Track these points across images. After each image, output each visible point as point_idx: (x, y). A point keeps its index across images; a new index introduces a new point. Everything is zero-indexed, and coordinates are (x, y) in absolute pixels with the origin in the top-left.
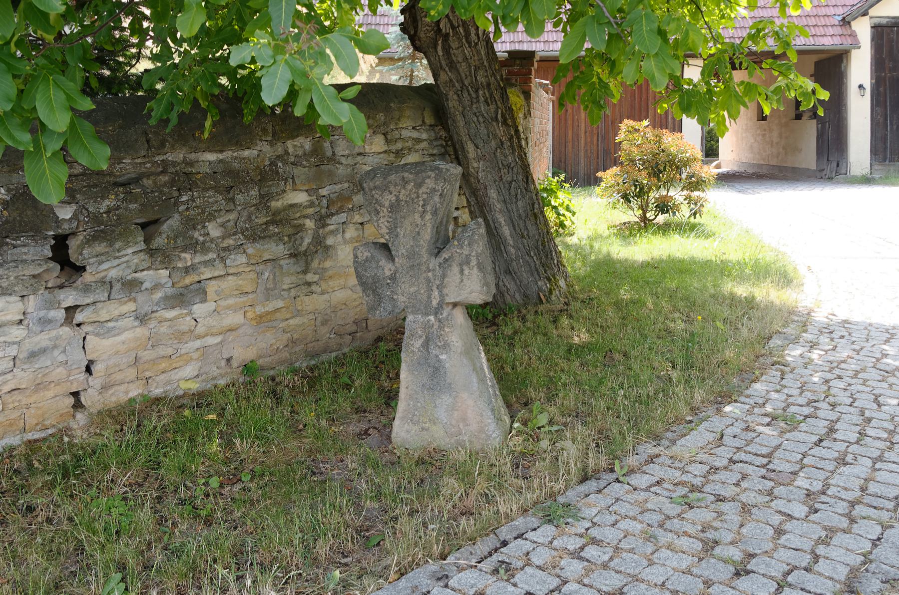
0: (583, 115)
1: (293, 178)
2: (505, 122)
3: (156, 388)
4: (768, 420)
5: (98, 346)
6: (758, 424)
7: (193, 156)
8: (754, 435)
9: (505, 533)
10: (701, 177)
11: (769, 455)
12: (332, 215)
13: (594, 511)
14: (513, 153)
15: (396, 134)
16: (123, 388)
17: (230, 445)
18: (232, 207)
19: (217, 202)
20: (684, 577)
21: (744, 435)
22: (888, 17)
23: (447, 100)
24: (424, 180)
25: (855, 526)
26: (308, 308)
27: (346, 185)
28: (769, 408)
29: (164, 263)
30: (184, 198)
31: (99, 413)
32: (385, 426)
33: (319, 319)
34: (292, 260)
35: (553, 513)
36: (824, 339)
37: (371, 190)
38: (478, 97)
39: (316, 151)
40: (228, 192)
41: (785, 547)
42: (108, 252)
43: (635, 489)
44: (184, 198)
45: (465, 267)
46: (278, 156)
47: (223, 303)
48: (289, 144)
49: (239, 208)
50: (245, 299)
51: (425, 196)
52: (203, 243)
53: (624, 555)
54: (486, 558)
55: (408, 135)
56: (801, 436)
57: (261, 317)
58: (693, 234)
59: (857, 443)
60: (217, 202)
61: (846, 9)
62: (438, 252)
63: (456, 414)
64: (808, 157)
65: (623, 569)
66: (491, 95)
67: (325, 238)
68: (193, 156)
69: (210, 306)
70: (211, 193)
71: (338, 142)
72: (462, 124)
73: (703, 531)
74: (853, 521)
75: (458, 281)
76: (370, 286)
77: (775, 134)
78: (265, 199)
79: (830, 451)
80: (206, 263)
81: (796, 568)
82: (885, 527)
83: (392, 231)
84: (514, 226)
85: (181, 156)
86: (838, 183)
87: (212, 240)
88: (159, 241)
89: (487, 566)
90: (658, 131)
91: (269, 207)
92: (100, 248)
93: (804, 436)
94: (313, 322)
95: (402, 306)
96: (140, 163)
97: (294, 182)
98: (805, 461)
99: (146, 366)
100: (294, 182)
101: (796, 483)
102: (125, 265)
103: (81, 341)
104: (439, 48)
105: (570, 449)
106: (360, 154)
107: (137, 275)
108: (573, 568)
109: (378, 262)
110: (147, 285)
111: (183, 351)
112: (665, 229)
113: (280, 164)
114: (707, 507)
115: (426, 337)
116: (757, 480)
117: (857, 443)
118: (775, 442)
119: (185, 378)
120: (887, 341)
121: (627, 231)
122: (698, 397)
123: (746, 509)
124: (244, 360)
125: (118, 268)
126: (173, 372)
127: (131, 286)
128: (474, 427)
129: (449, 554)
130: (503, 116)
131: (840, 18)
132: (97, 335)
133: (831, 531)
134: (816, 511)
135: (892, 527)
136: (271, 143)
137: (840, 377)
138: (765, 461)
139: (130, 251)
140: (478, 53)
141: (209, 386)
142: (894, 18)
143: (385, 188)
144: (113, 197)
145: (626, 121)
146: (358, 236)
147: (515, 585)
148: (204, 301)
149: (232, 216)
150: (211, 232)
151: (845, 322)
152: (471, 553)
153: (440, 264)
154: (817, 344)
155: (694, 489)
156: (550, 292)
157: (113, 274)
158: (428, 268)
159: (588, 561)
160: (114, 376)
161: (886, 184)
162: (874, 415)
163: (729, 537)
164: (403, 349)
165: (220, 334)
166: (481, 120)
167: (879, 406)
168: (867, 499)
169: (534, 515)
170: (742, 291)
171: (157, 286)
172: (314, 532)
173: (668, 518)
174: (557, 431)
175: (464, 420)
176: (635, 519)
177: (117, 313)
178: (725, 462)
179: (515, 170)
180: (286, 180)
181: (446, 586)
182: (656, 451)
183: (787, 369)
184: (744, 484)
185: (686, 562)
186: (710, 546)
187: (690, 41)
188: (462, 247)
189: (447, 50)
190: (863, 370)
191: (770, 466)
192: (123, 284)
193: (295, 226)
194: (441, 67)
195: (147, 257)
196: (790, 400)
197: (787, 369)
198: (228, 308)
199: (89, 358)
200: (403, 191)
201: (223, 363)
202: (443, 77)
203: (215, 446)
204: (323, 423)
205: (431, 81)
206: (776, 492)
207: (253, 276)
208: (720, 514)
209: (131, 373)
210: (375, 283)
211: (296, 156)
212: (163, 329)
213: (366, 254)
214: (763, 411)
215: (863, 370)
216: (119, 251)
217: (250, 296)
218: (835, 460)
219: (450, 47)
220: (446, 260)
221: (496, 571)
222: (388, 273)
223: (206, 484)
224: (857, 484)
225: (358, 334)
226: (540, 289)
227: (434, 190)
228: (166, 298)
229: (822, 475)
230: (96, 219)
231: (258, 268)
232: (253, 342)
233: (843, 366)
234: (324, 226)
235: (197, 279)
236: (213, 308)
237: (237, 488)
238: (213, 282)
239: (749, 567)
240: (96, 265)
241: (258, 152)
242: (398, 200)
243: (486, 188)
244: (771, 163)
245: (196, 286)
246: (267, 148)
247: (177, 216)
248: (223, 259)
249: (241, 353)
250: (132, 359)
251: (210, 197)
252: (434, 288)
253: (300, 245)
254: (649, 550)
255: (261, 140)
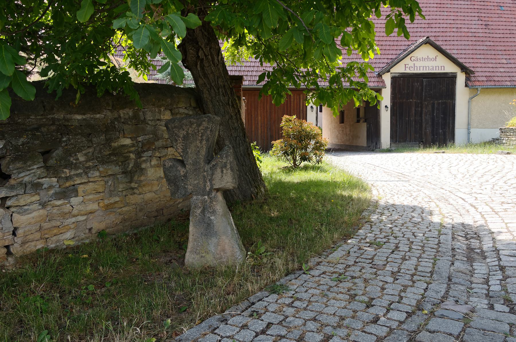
0: (260, 118)
1: (123, 130)
2: (233, 106)
3: (51, 244)
4: (368, 245)
5: (20, 219)
6: (365, 247)
7: (69, 116)
8: (364, 251)
9: (252, 299)
10: (322, 143)
11: (372, 259)
12: (144, 151)
13: (295, 287)
14: (237, 122)
15: (176, 110)
16: (33, 244)
17: (97, 269)
18: (91, 145)
19: (82, 142)
20: (343, 310)
21: (359, 251)
22: (399, 73)
23: (203, 93)
24: (202, 122)
25: (415, 284)
26: (132, 202)
27: (151, 136)
28: (368, 240)
29: (54, 174)
30: (64, 139)
31: (21, 257)
32: (180, 258)
33: (138, 208)
34: (123, 176)
35: (274, 289)
36: (386, 212)
37: (173, 128)
38: (219, 92)
39: (136, 116)
40: (89, 137)
41: (387, 294)
42: (23, 167)
43: (313, 276)
44: (64, 139)
45: (224, 169)
46: (115, 118)
47: (87, 198)
48: (121, 112)
49: (95, 146)
50: (99, 196)
51: (202, 131)
52: (76, 164)
53: (313, 303)
54: (245, 310)
55: (183, 111)
56: (385, 250)
57: (107, 206)
58: (319, 171)
59: (409, 251)
60: (82, 142)
61: (380, 69)
62: (209, 162)
63: (219, 247)
64: (363, 141)
65: (314, 309)
66: (226, 92)
67: (141, 164)
68: (69, 116)
69: (80, 199)
70: (79, 137)
71: (147, 113)
72: (211, 106)
73: (348, 291)
74: (414, 282)
75: (220, 176)
76: (173, 181)
77: (348, 130)
78: (109, 141)
79: (398, 256)
80: (77, 175)
81: (393, 302)
82: (428, 283)
83: (185, 150)
84: (238, 160)
85: (62, 116)
86: (376, 152)
87: (80, 163)
88: (52, 162)
89: (245, 313)
90: (301, 121)
91: (111, 146)
92: (19, 165)
93: (385, 251)
94: (135, 210)
95: (190, 191)
96: (40, 119)
97: (124, 133)
98: (388, 260)
99: (46, 231)
100: (124, 133)
101: (386, 269)
102: (33, 174)
103: (10, 217)
104: (198, 66)
105: (279, 262)
106: (158, 120)
107: (40, 180)
108: (290, 311)
109: (177, 168)
110: (45, 186)
111: (66, 224)
112: (306, 168)
113: (116, 123)
114: (348, 281)
115: (203, 207)
116: (369, 269)
117: (409, 251)
118: (374, 253)
119: (67, 238)
120: (412, 212)
121: (288, 170)
122: (336, 236)
123: (366, 281)
124: (99, 230)
125: (29, 176)
126: (60, 235)
127: (37, 187)
128: (229, 254)
129: (225, 310)
130: (232, 103)
131: (377, 73)
132: (19, 213)
133: (406, 287)
134: (397, 279)
135: (431, 283)
136: (111, 111)
137: (396, 226)
138: (371, 261)
139: (35, 167)
140: (219, 69)
141: (80, 244)
142: (401, 73)
143: (180, 127)
144: (25, 137)
145: (285, 115)
146: (158, 164)
147: (262, 320)
148: (77, 196)
149: (91, 150)
150: (80, 158)
151: (393, 205)
152: (237, 309)
153: (211, 167)
154: (383, 213)
155: (340, 274)
156: (257, 194)
157: (26, 179)
158: (204, 170)
159: (296, 307)
160: (28, 236)
161: (397, 152)
162: (414, 240)
163: (361, 293)
164: (191, 214)
165: (86, 215)
166: (221, 104)
167: (415, 236)
168: (418, 273)
169: (266, 290)
170: (345, 193)
171: (51, 187)
172: (150, 307)
173: (331, 287)
174: (270, 255)
175: (224, 250)
176: (316, 288)
177: (29, 201)
178: (353, 263)
179: (239, 131)
180: (119, 132)
181: (227, 324)
182: (320, 260)
183: (373, 224)
184: (363, 271)
185: (343, 304)
186: (353, 297)
187: (346, 40)
188: (222, 158)
189: (202, 67)
190: (405, 223)
191: (373, 263)
192: (32, 185)
193: (125, 157)
194: (200, 76)
195: (45, 170)
196: (377, 236)
197: (373, 224)
198: (90, 200)
199: (14, 226)
200: (190, 129)
201: (87, 231)
202: (200, 82)
203: (88, 270)
204: (147, 257)
205: (193, 86)
206: (378, 273)
207: (102, 183)
208: (355, 284)
209: (38, 235)
210: (175, 179)
211: (125, 119)
212: (55, 211)
213: (170, 164)
214: (365, 241)
215: (405, 223)
216: (29, 166)
217: (102, 194)
218: (401, 259)
219: (204, 66)
220: (214, 166)
221: (251, 315)
222: (182, 174)
223: (86, 289)
224: (413, 267)
225: (158, 217)
226: (252, 192)
227: (207, 128)
228: (56, 194)
229: (397, 265)
230: (16, 148)
231: (106, 179)
232: (104, 220)
233: (396, 222)
234: (141, 157)
235: (72, 183)
236: (81, 200)
237: (103, 290)
238: (82, 186)
239: (372, 304)
240: (17, 174)
241: (104, 115)
242: (188, 134)
243: (224, 140)
244: (347, 144)
245: (72, 188)
246: (109, 113)
247: (61, 148)
248: (86, 173)
249: (97, 225)
250: (38, 227)
251: (78, 139)
252: (208, 181)
253: (128, 167)
254: (325, 301)
255: (106, 109)
